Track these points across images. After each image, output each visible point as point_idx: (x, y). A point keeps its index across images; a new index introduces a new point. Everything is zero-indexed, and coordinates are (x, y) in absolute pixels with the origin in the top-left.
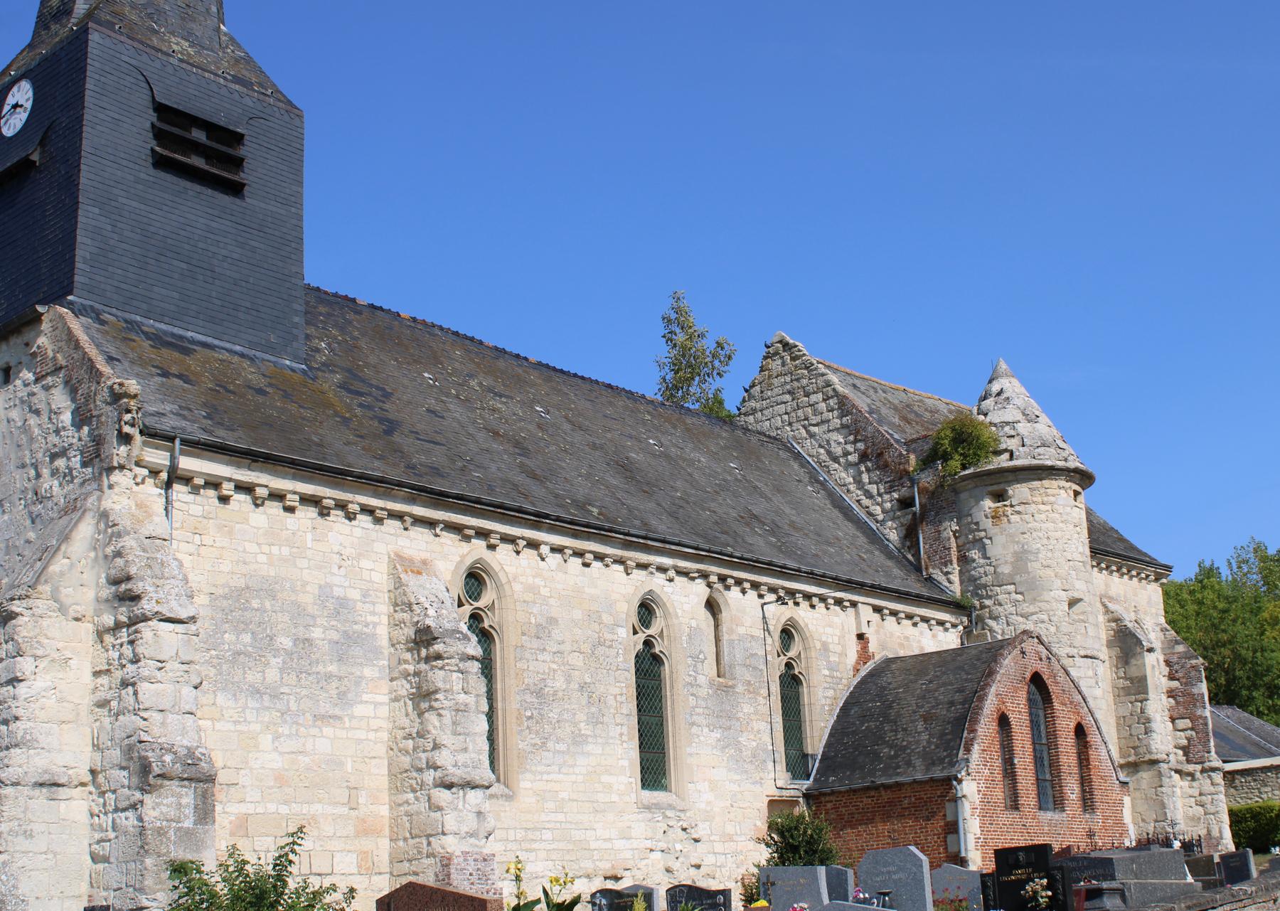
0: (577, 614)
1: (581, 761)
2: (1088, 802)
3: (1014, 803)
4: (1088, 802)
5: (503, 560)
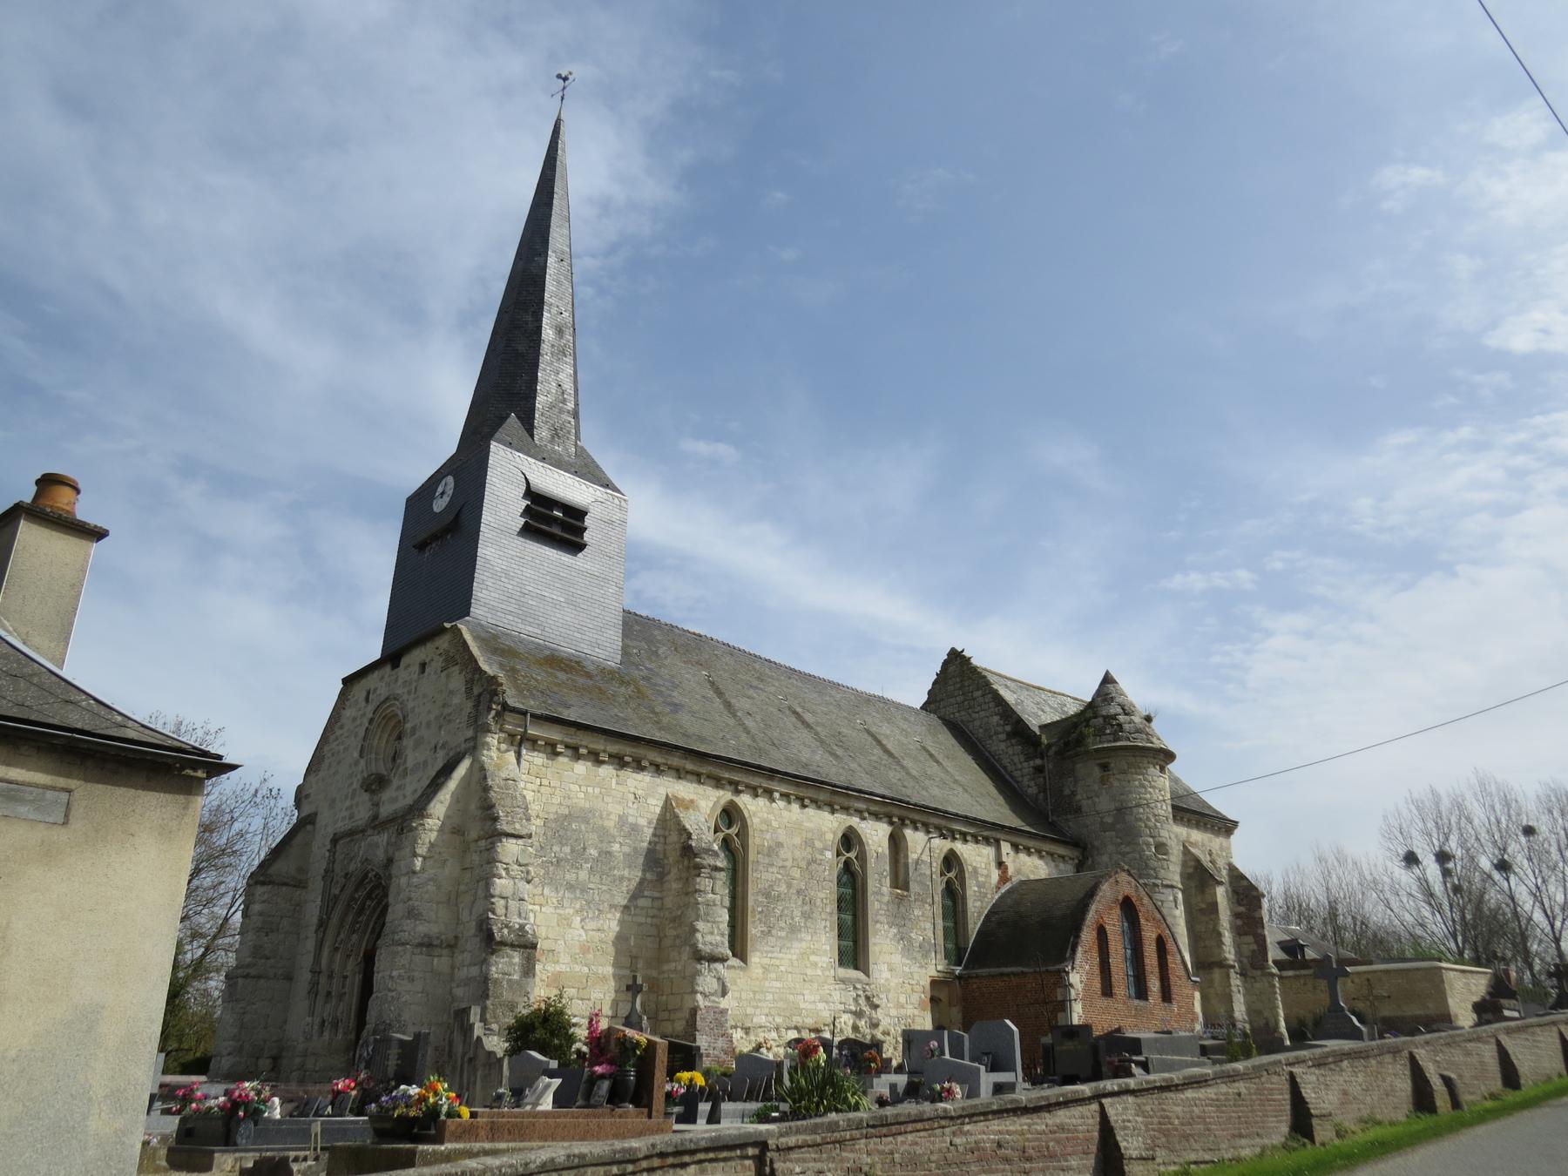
0: (797, 841)
1: (796, 944)
2: (1166, 996)
3: (1107, 990)
4: (1166, 996)
5: (745, 801)
